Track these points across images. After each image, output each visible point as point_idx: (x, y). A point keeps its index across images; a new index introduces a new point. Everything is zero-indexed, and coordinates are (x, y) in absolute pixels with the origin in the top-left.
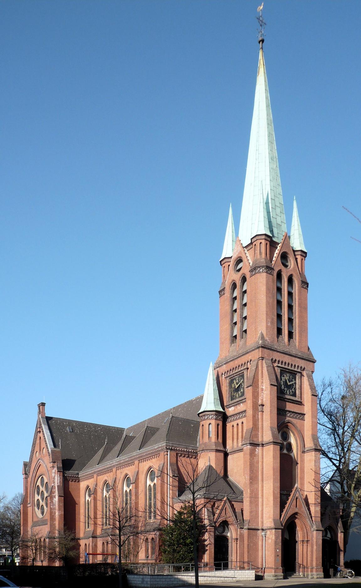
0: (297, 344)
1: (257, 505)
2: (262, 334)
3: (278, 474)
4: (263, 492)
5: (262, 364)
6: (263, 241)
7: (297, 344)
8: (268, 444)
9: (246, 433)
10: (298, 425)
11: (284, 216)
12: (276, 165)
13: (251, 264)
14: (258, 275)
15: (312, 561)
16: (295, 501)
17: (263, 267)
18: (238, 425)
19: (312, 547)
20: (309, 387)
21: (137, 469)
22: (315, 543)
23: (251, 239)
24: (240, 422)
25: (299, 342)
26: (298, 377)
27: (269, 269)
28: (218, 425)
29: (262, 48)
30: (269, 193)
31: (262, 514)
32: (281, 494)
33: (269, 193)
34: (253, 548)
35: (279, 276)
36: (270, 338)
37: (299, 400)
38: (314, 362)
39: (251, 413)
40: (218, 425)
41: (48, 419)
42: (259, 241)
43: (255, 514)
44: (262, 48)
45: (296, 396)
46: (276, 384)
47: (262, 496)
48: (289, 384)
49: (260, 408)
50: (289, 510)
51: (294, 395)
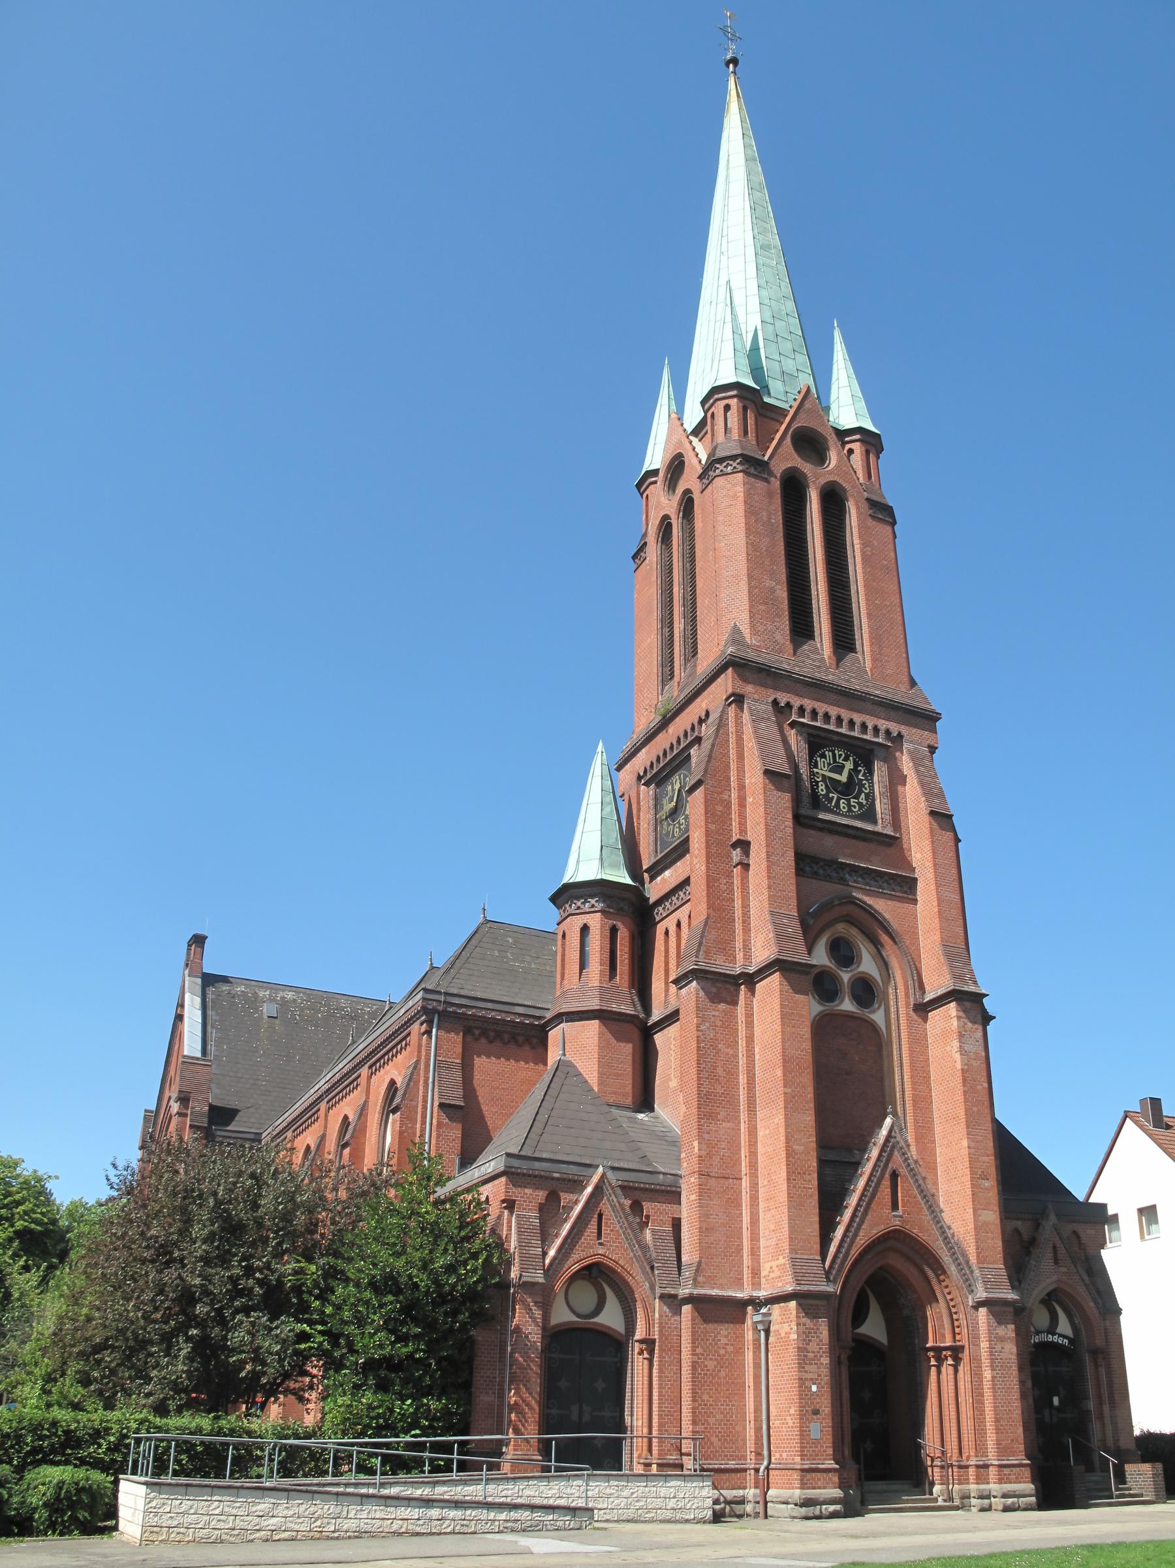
0: (868, 665)
1: (736, 1203)
2: (736, 630)
3: (807, 1080)
4: (753, 1154)
5: (738, 720)
6: (734, 402)
7: (868, 665)
8: (765, 971)
9: (688, 940)
10: (895, 924)
11: (803, 359)
12: (776, 260)
13: (703, 462)
14: (719, 482)
15: (979, 1431)
16: (886, 1183)
17: (733, 458)
18: (679, 925)
19: (976, 1374)
20: (919, 790)
21: (363, 1099)
22: (985, 1362)
23: (703, 403)
24: (682, 914)
25: (874, 660)
26: (880, 771)
27: (754, 466)
28: (614, 931)
29: (734, 72)
30: (759, 328)
31: (755, 1238)
32: (822, 1163)
33: (759, 328)
34: (717, 1382)
35: (793, 488)
36: (771, 643)
37: (889, 831)
38: (927, 719)
39: (704, 868)
40: (614, 931)
41: (209, 980)
42: (721, 404)
43: (724, 1240)
44: (734, 72)
45: (875, 822)
46: (1091, 1201)
47: (753, 1165)
48: (843, 778)
49: (736, 855)
50: (863, 1219)
51: (869, 814)
